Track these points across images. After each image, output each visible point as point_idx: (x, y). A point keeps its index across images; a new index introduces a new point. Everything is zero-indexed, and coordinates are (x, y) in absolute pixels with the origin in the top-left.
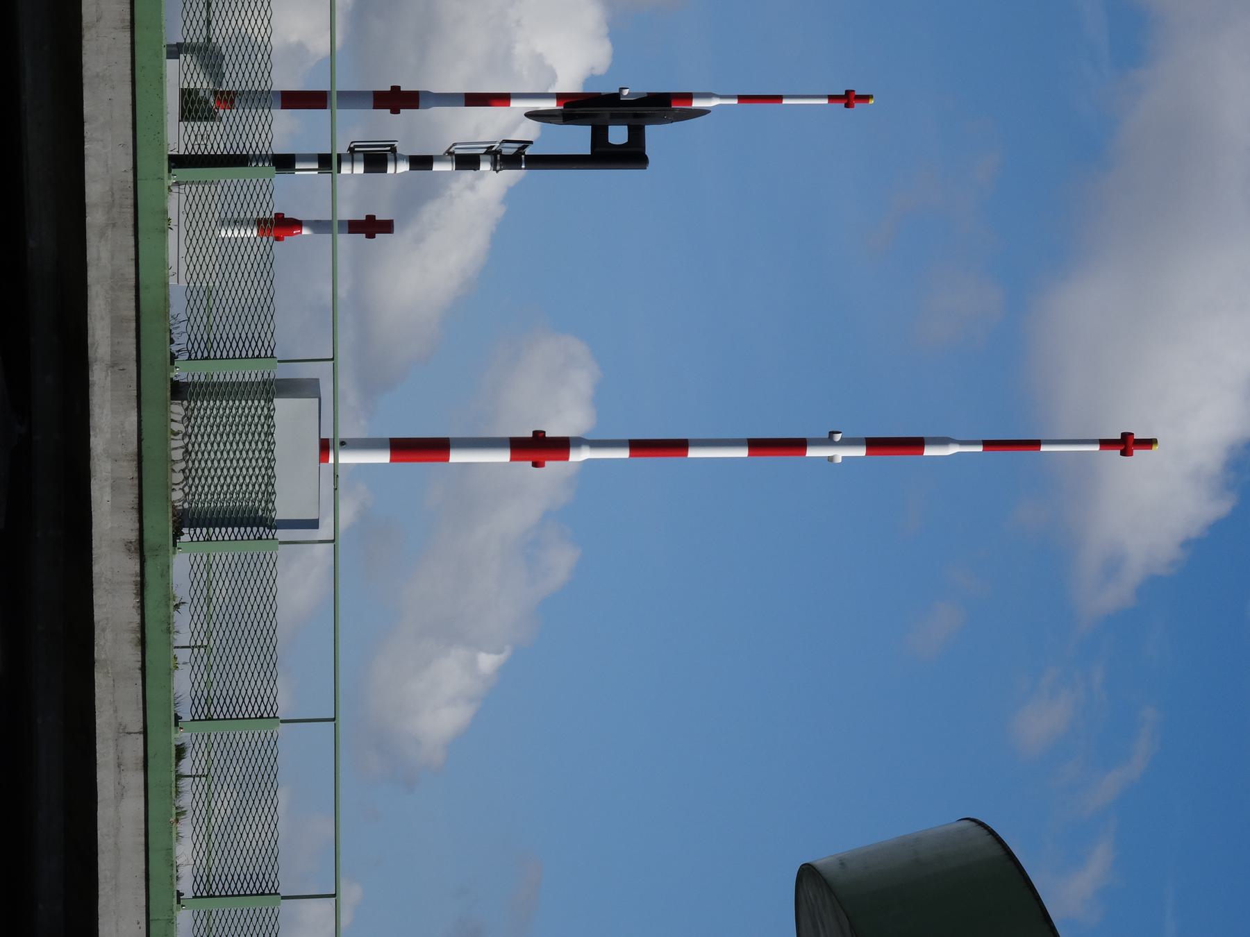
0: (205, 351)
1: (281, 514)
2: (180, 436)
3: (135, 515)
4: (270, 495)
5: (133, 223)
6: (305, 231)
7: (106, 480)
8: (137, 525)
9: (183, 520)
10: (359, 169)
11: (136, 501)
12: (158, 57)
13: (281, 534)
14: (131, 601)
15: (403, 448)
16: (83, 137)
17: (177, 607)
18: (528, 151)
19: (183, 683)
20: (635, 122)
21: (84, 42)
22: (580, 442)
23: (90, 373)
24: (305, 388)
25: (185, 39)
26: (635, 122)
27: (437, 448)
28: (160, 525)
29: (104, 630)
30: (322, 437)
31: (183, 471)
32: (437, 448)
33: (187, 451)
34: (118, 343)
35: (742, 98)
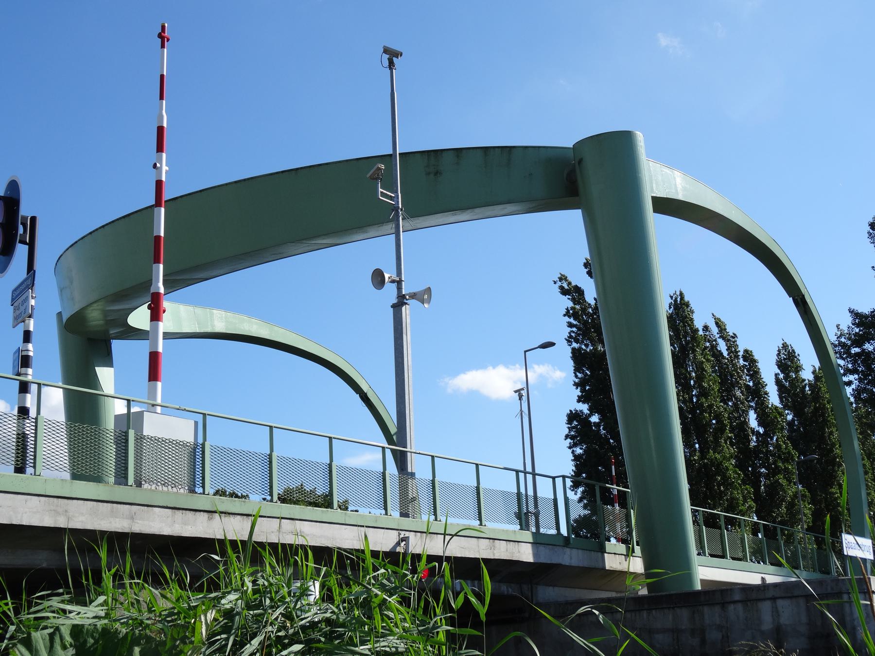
2: (157, 487)
3: (198, 513)
4: (185, 445)
5: (66, 500)
7: (182, 527)
8: (202, 513)
11: (192, 512)
15: (154, 375)
25: (12, 464)
31: (172, 487)
33: (164, 484)
34: (123, 515)
35: (162, 97)
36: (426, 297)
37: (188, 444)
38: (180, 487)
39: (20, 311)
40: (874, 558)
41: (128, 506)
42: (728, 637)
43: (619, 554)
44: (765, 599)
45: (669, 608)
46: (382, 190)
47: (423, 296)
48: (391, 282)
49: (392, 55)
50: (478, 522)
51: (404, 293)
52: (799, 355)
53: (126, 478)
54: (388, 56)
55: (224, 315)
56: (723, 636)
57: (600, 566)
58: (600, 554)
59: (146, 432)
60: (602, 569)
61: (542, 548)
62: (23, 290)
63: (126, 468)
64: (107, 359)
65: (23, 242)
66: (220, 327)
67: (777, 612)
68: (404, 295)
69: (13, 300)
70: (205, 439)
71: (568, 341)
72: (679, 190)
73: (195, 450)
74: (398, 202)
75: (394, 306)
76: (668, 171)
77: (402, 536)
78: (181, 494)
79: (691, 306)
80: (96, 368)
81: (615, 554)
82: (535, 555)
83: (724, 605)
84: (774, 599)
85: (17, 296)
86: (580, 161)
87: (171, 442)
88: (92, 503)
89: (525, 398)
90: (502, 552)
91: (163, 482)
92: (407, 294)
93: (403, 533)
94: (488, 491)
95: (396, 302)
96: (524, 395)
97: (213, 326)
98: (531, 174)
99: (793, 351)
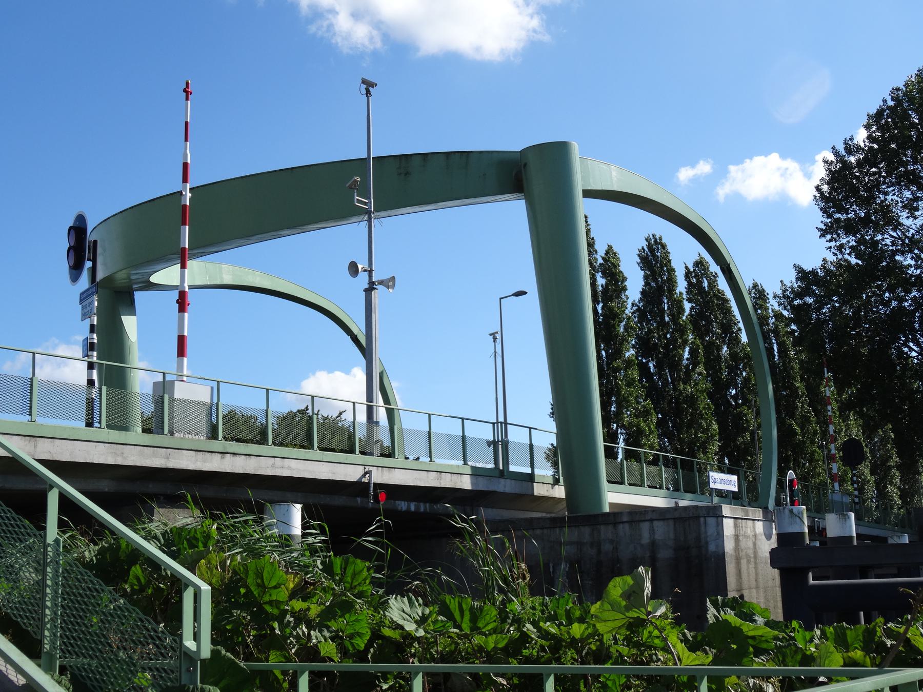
3: (214, 454)
4: (204, 404)
8: (216, 454)
12: (65, 429)
14: (238, 458)
15: (181, 352)
16: (92, 463)
21: (58, 460)
29: (245, 470)
30: (175, 382)
35: (186, 140)
36: (391, 284)
37: (206, 404)
38: (200, 435)
39: (87, 310)
40: (566, 496)
41: (164, 449)
42: (617, 548)
43: (547, 484)
45: (575, 526)
46: (358, 198)
47: (389, 283)
48: (364, 271)
49: (369, 85)
50: (429, 459)
51: (374, 280)
52: (768, 294)
53: (163, 429)
54: (365, 86)
55: (231, 269)
56: (613, 548)
57: (530, 493)
58: (530, 483)
59: (177, 395)
61: (480, 479)
62: (89, 295)
63: (163, 422)
64: (131, 307)
65: (89, 260)
66: (228, 280)
67: (654, 530)
68: (374, 282)
69: (81, 300)
70: (218, 400)
72: (614, 182)
73: (211, 408)
74: (371, 206)
75: (366, 290)
76: (604, 167)
77: (367, 470)
78: (202, 440)
79: (668, 247)
80: (122, 317)
81: (543, 483)
82: (472, 484)
83: (615, 524)
84: (651, 520)
85: (84, 299)
86: (525, 165)
87: (194, 402)
88: (140, 447)
89: (499, 340)
90: (447, 482)
91: (188, 432)
92: (376, 282)
93: (367, 467)
94: (438, 434)
95: (368, 287)
96: (498, 337)
97: (222, 278)
98: (484, 175)
99: (763, 289)
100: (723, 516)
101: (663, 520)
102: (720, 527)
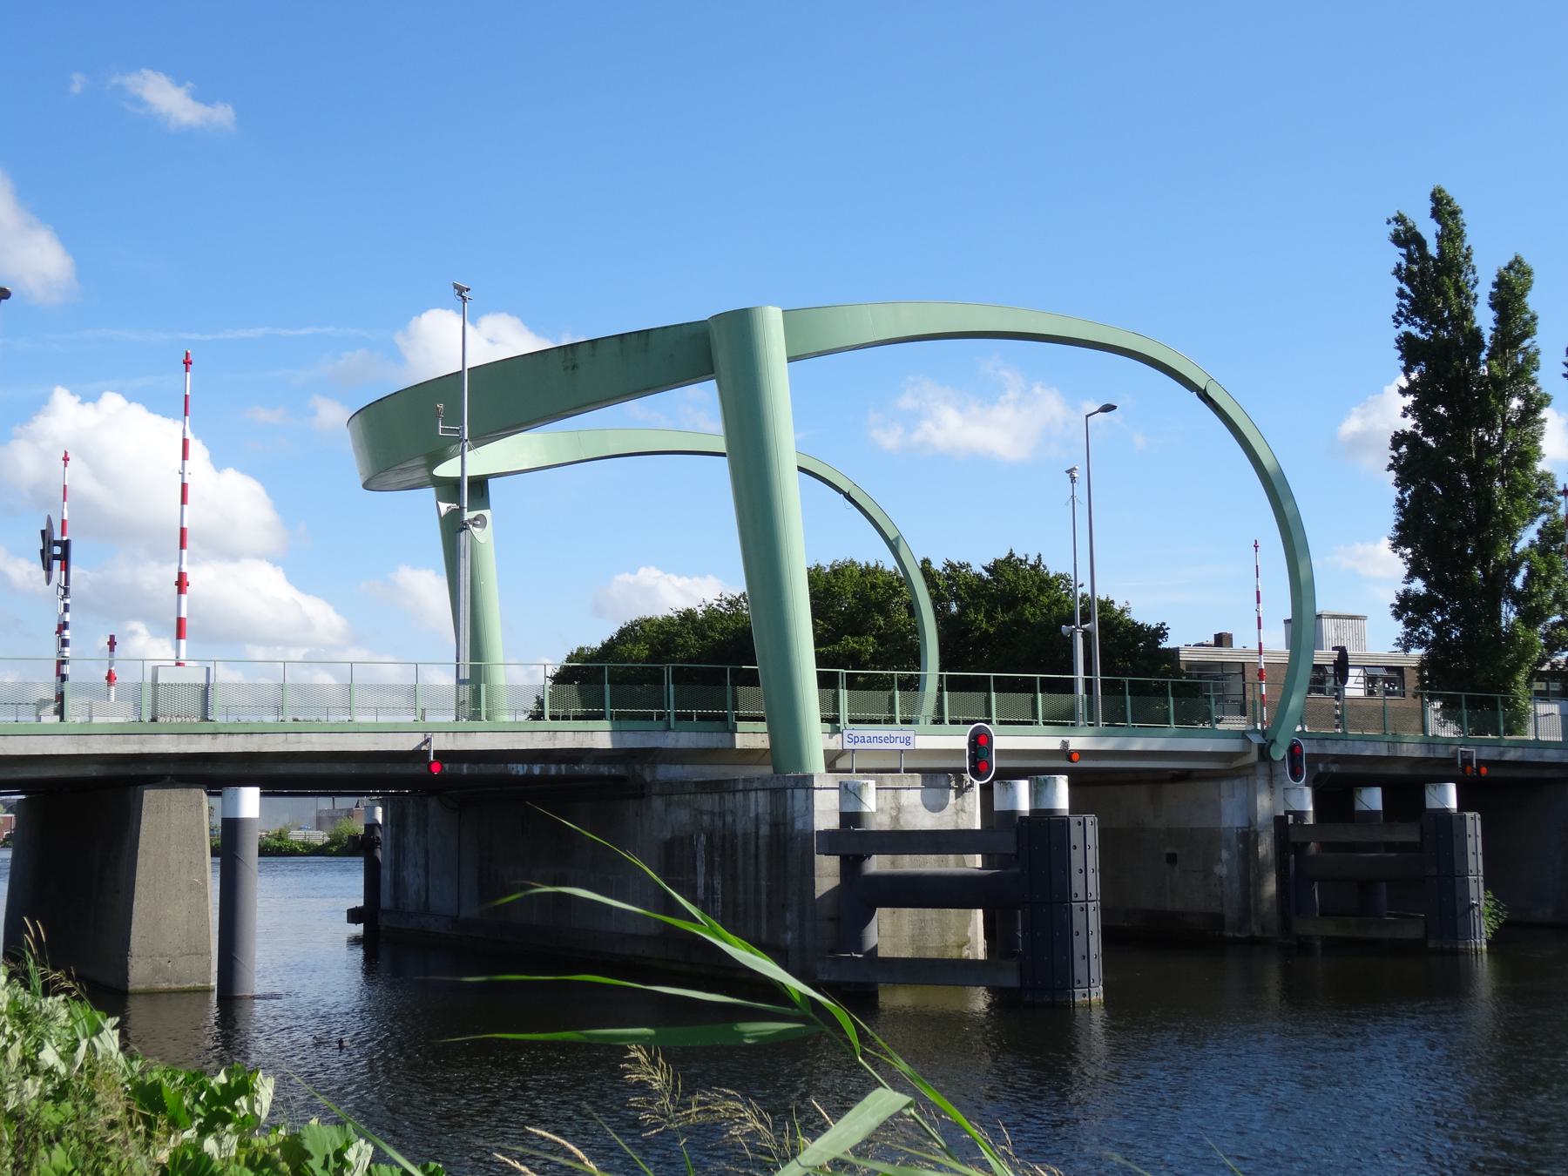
0: (138, 707)
1: (204, 682)
3: (202, 736)
6: (113, 668)
9: (205, 718)
10: (67, 649)
13: (212, 681)
17: (239, 721)
18: (63, 584)
19: (270, 719)
20: (52, 544)
22: (180, 568)
23: (1273, 847)
24: (155, 670)
26: (52, 544)
27: (180, 622)
28: (206, 727)
32: (180, 622)
44: (751, 790)
58: (728, 735)
60: (730, 749)
71: (1396, 320)
82: (613, 741)
100: (814, 788)
101: (764, 789)
102: (810, 801)
